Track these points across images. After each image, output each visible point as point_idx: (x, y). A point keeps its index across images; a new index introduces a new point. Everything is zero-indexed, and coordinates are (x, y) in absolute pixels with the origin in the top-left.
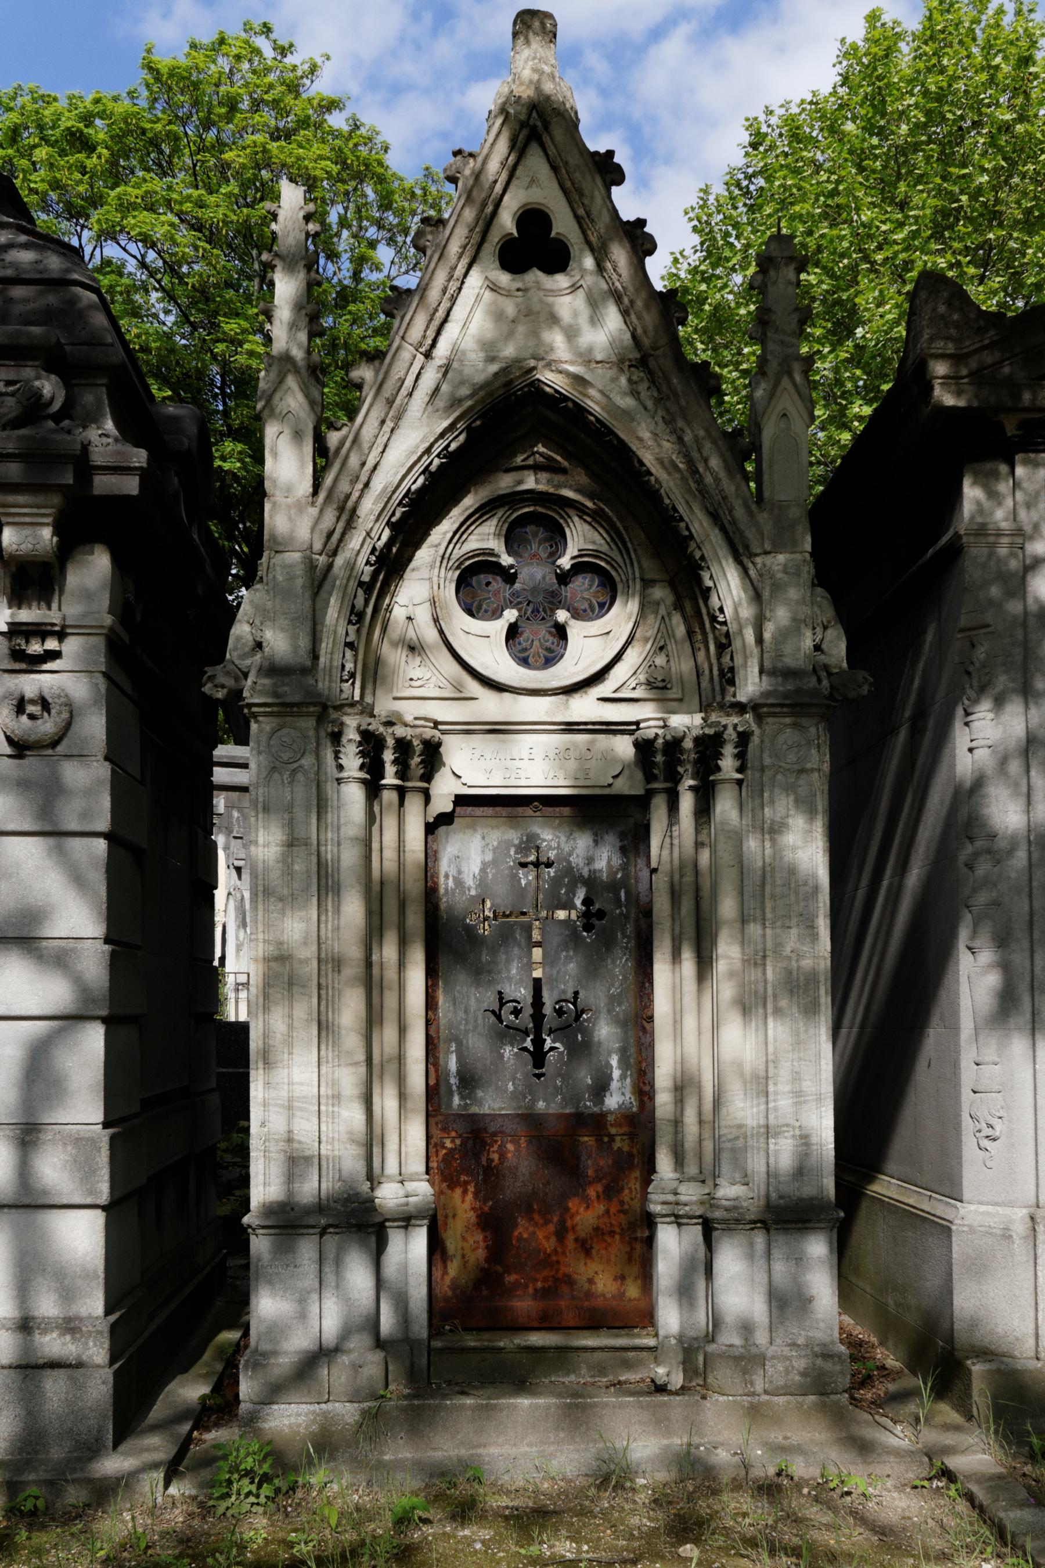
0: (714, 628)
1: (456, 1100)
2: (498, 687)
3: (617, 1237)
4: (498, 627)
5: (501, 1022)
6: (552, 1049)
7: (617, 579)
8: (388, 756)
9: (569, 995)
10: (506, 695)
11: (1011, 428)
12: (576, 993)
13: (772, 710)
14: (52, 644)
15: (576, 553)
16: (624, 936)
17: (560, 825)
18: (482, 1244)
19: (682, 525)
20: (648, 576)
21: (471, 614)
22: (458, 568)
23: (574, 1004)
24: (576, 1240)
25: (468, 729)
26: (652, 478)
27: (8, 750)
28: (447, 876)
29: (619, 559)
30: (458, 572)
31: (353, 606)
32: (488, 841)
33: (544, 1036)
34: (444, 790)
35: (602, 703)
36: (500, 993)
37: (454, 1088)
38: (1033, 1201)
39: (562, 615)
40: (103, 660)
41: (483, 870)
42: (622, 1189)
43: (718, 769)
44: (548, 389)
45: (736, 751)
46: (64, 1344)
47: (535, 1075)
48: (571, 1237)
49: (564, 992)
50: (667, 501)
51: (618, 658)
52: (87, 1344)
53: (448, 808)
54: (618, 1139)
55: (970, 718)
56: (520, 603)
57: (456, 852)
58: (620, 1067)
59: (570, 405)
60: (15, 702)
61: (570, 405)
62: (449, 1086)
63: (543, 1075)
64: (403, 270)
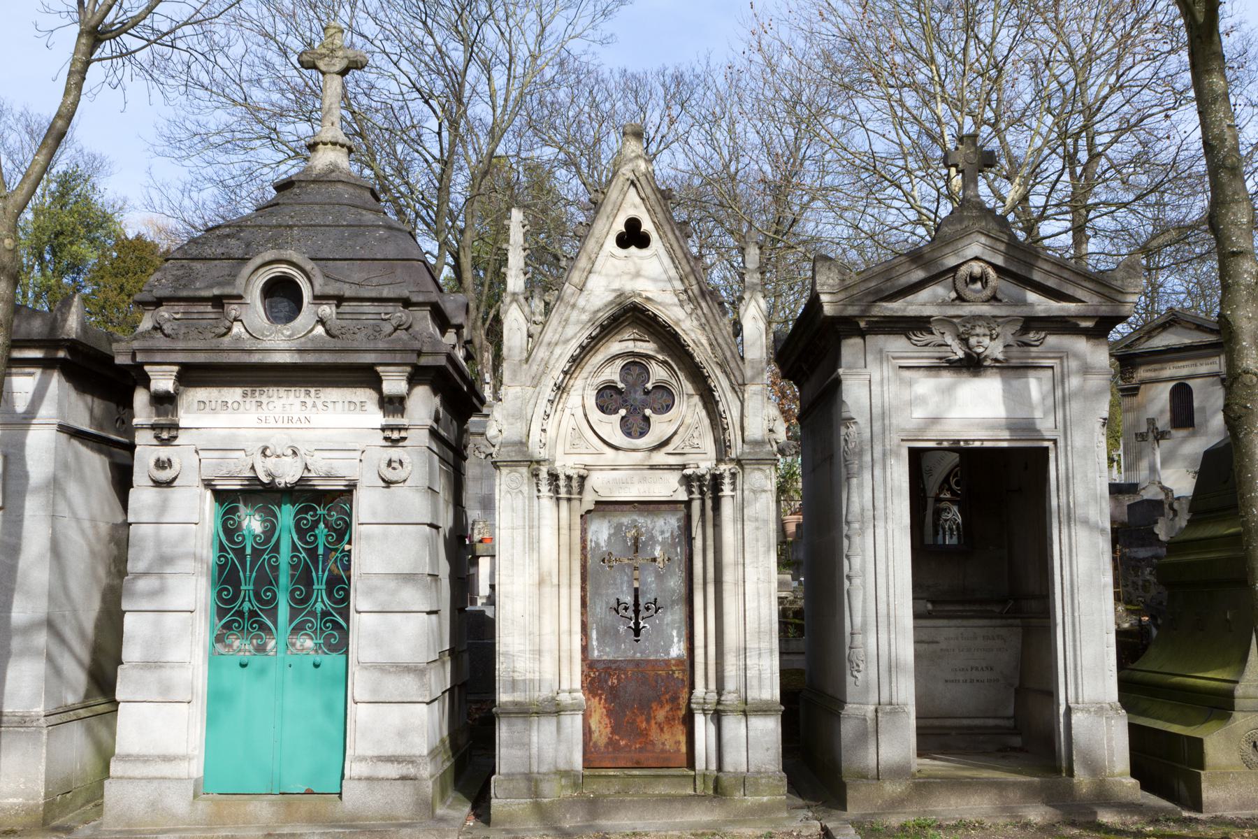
1: (596, 653)
2: (616, 448)
8: (562, 483)
11: (862, 324)
14: (403, 434)
27: (383, 484)
39: (648, 412)
48: (653, 722)
51: (675, 433)
53: (592, 507)
64: (891, 191)
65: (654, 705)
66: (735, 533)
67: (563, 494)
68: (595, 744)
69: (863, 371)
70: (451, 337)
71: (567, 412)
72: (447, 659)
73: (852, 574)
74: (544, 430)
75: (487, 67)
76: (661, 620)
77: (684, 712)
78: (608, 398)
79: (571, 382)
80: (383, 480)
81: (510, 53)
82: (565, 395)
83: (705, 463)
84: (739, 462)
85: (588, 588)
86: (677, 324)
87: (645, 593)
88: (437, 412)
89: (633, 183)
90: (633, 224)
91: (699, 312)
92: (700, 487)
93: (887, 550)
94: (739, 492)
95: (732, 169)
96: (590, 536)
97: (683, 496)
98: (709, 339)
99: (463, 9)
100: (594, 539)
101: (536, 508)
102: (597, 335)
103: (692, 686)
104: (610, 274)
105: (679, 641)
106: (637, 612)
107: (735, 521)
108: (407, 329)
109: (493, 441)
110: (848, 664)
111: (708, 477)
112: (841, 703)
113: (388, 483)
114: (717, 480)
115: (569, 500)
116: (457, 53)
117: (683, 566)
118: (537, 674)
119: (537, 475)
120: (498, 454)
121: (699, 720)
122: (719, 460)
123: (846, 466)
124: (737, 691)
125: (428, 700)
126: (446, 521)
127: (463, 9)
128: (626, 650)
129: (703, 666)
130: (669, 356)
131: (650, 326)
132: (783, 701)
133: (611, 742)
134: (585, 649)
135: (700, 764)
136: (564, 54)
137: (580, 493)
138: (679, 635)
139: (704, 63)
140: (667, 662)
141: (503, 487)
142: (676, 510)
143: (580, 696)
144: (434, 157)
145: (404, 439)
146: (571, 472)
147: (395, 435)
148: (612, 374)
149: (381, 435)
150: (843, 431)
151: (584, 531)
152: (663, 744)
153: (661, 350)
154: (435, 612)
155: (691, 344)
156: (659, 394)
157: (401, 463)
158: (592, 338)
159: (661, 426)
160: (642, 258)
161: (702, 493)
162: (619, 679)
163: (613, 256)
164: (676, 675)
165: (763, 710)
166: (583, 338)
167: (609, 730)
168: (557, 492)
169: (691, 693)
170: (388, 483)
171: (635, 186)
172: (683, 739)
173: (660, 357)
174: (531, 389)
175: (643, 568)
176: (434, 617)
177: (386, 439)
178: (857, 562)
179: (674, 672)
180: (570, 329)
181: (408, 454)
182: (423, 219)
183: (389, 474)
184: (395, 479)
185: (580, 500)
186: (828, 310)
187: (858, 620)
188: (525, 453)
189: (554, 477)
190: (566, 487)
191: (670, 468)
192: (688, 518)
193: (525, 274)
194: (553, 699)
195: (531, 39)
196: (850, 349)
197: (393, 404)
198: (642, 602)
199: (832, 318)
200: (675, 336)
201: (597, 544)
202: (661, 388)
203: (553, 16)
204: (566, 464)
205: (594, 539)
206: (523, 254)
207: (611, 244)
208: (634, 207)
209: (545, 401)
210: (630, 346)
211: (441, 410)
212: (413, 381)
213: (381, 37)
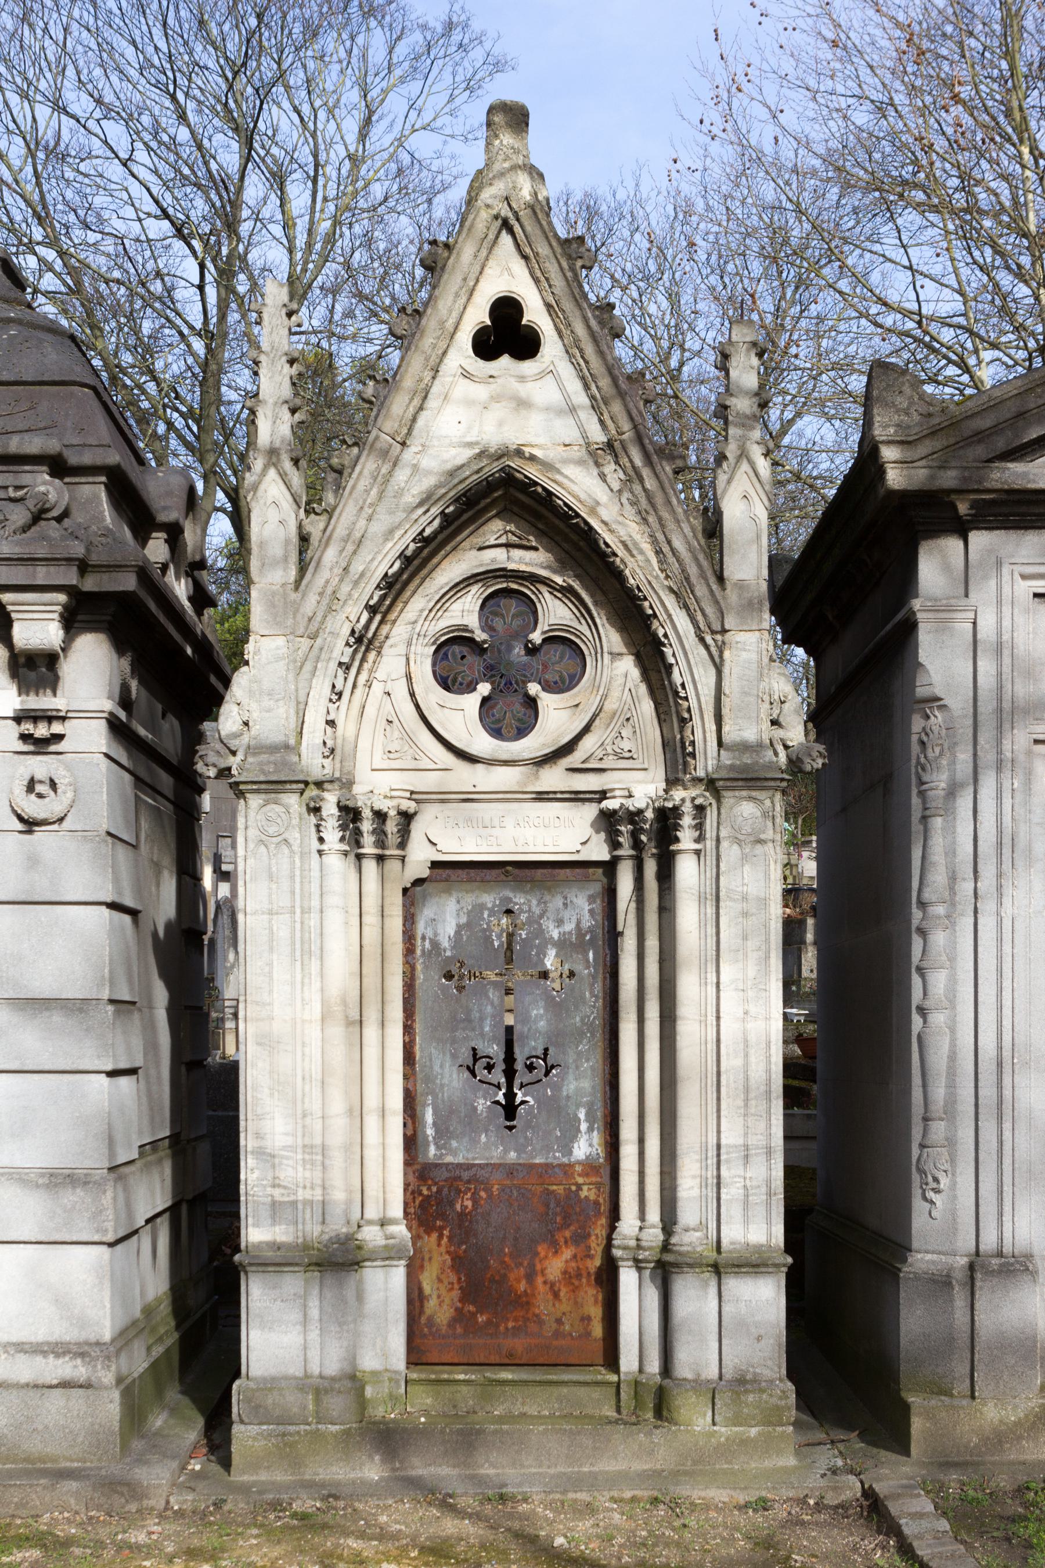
0: (677, 704)
1: (432, 1150)
3: (584, 1280)
4: (471, 702)
5: (475, 1076)
6: (523, 1102)
7: (586, 652)
8: (367, 826)
9: (540, 1052)
10: (479, 766)
11: (963, 508)
12: (546, 1050)
13: (729, 784)
14: (57, 728)
15: (546, 628)
16: (592, 995)
17: (531, 889)
18: (456, 1286)
19: (646, 604)
20: (616, 650)
21: (447, 688)
22: (434, 643)
23: (545, 1060)
24: (545, 1283)
25: (443, 798)
26: (618, 560)
27: (20, 826)
28: (423, 938)
29: (588, 633)
30: (434, 648)
31: (334, 686)
32: (463, 903)
33: (516, 1091)
34: (419, 856)
35: (570, 774)
36: (474, 1049)
37: (430, 1138)
38: (973, 1250)
39: (533, 688)
40: (104, 742)
41: (458, 933)
42: (589, 1235)
43: (677, 840)
44: (518, 475)
45: (694, 823)
46: (75, 1367)
47: (507, 1127)
48: (540, 1280)
49: (535, 1048)
50: (632, 581)
51: (586, 729)
52: (95, 1366)
53: (425, 873)
54: (585, 1188)
55: (924, 787)
56: (493, 676)
57: (432, 916)
58: (587, 1120)
59: (540, 490)
60: (25, 783)
61: (540, 490)
62: (426, 1137)
63: (514, 1127)
65: (542, 1249)
66: (702, 924)
67: (369, 848)
68: (430, 1319)
69: (964, 602)
70: (157, 549)
71: (377, 688)
72: (165, 1152)
73: (927, 1004)
74: (331, 723)
75: (278, 180)
76: (557, 1088)
77: (598, 1262)
78: (456, 660)
79: (385, 630)
80: (20, 818)
81: (315, 155)
82: (372, 656)
83: (643, 788)
84: (711, 784)
85: (418, 1027)
86: (593, 511)
87: (524, 1038)
88: (125, 688)
89: (506, 225)
90: (506, 309)
91: (637, 488)
92: (635, 835)
93: (1000, 959)
94: (710, 844)
95: (674, 363)
96: (421, 928)
97: (599, 852)
98: (654, 541)
99: (236, 74)
100: (429, 934)
101: (315, 873)
102: (435, 534)
103: (615, 1215)
104: (467, 414)
105: (590, 1129)
106: (510, 1073)
107: (701, 899)
108: (59, 519)
109: (233, 744)
110: (916, 1177)
111: (649, 814)
112: (901, 1248)
113: (30, 825)
114: (667, 820)
115: (380, 859)
116: (227, 154)
117: (598, 988)
118: (318, 1191)
119: (317, 810)
120: (241, 768)
121: (628, 1279)
122: (672, 782)
123: (922, 794)
124: (702, 1226)
125: (110, 1237)
126: (165, 906)
127: (236, 74)
128: (486, 1149)
129: (635, 1167)
130: (577, 576)
131: (539, 516)
132: (790, 1246)
133: (459, 1316)
134: (411, 1143)
135: (628, 1361)
136: (406, 159)
137: (402, 845)
138: (590, 1118)
139: (630, 184)
140: (567, 1169)
141: (252, 833)
142: (587, 879)
143: (401, 1230)
144: (191, 328)
145: (59, 738)
146: (383, 805)
147: (42, 731)
148: (466, 612)
149: (13, 731)
150: (917, 724)
151: (409, 919)
152: (559, 1321)
153: (563, 565)
154: (132, 1072)
155: (620, 552)
156: (555, 652)
157: (53, 785)
158: (424, 540)
159: (556, 717)
160: (522, 379)
161: (637, 845)
162: (475, 1200)
163: (466, 375)
164: (584, 1193)
165: (751, 1264)
166: (404, 541)
167: (456, 1293)
168: (358, 844)
169: (612, 1228)
170: (30, 825)
171: (511, 231)
172: (596, 1312)
173: (559, 580)
174: (305, 643)
175: (520, 988)
176: (125, 1083)
177: (25, 738)
178: (938, 981)
179: (579, 1187)
180: (383, 512)
181: (68, 768)
182: (177, 431)
183: (33, 807)
184: (41, 815)
185: (403, 859)
186: (895, 478)
187: (939, 1093)
188: (291, 767)
189: (350, 814)
190: (370, 832)
191: (577, 797)
192: (611, 893)
193: (293, 411)
194: (350, 1238)
195: (351, 127)
196: (935, 566)
197: (36, 669)
198: (520, 1055)
199: (904, 496)
200: (588, 534)
201: (435, 945)
202: (560, 641)
203: (385, 92)
204: (378, 786)
205: (429, 934)
206: (288, 371)
207: (462, 352)
208: (507, 275)
209: (333, 665)
210: (498, 558)
211: (134, 684)
212: (76, 618)
213: (97, 114)
